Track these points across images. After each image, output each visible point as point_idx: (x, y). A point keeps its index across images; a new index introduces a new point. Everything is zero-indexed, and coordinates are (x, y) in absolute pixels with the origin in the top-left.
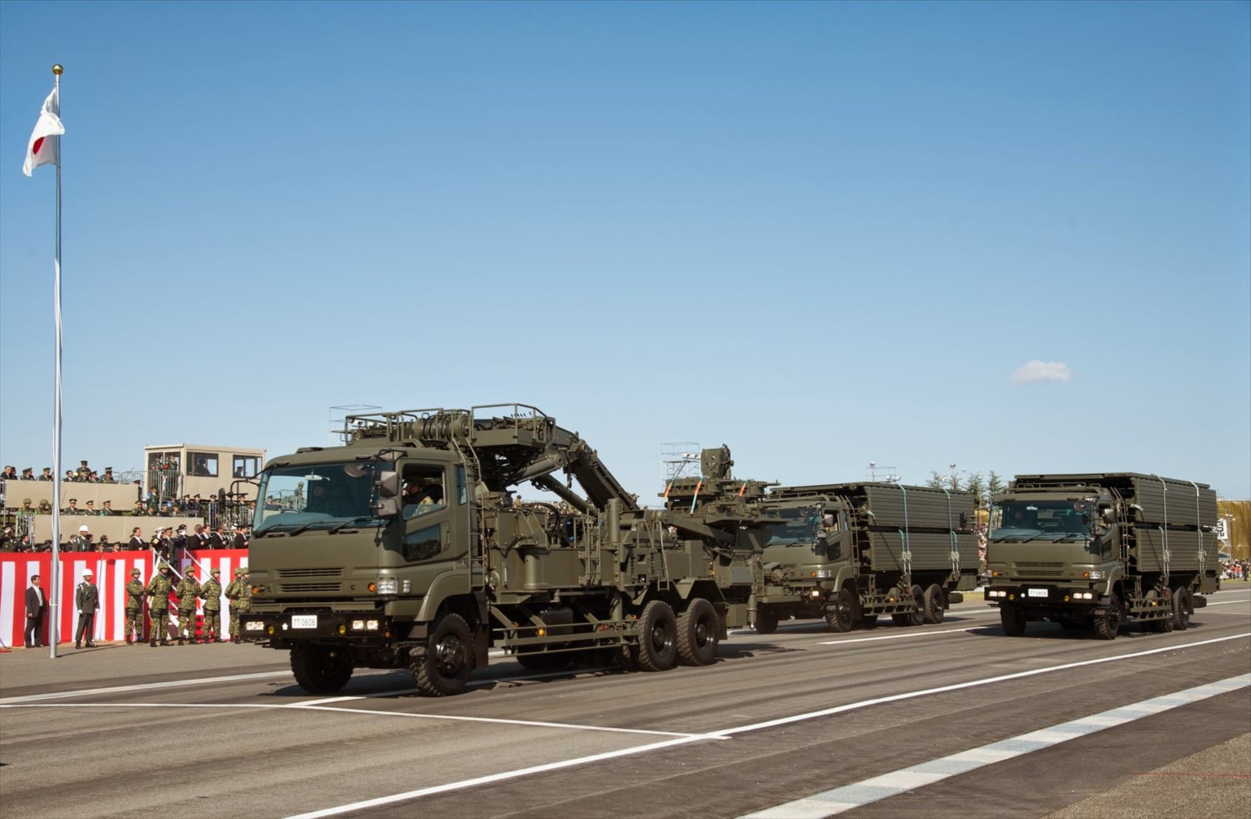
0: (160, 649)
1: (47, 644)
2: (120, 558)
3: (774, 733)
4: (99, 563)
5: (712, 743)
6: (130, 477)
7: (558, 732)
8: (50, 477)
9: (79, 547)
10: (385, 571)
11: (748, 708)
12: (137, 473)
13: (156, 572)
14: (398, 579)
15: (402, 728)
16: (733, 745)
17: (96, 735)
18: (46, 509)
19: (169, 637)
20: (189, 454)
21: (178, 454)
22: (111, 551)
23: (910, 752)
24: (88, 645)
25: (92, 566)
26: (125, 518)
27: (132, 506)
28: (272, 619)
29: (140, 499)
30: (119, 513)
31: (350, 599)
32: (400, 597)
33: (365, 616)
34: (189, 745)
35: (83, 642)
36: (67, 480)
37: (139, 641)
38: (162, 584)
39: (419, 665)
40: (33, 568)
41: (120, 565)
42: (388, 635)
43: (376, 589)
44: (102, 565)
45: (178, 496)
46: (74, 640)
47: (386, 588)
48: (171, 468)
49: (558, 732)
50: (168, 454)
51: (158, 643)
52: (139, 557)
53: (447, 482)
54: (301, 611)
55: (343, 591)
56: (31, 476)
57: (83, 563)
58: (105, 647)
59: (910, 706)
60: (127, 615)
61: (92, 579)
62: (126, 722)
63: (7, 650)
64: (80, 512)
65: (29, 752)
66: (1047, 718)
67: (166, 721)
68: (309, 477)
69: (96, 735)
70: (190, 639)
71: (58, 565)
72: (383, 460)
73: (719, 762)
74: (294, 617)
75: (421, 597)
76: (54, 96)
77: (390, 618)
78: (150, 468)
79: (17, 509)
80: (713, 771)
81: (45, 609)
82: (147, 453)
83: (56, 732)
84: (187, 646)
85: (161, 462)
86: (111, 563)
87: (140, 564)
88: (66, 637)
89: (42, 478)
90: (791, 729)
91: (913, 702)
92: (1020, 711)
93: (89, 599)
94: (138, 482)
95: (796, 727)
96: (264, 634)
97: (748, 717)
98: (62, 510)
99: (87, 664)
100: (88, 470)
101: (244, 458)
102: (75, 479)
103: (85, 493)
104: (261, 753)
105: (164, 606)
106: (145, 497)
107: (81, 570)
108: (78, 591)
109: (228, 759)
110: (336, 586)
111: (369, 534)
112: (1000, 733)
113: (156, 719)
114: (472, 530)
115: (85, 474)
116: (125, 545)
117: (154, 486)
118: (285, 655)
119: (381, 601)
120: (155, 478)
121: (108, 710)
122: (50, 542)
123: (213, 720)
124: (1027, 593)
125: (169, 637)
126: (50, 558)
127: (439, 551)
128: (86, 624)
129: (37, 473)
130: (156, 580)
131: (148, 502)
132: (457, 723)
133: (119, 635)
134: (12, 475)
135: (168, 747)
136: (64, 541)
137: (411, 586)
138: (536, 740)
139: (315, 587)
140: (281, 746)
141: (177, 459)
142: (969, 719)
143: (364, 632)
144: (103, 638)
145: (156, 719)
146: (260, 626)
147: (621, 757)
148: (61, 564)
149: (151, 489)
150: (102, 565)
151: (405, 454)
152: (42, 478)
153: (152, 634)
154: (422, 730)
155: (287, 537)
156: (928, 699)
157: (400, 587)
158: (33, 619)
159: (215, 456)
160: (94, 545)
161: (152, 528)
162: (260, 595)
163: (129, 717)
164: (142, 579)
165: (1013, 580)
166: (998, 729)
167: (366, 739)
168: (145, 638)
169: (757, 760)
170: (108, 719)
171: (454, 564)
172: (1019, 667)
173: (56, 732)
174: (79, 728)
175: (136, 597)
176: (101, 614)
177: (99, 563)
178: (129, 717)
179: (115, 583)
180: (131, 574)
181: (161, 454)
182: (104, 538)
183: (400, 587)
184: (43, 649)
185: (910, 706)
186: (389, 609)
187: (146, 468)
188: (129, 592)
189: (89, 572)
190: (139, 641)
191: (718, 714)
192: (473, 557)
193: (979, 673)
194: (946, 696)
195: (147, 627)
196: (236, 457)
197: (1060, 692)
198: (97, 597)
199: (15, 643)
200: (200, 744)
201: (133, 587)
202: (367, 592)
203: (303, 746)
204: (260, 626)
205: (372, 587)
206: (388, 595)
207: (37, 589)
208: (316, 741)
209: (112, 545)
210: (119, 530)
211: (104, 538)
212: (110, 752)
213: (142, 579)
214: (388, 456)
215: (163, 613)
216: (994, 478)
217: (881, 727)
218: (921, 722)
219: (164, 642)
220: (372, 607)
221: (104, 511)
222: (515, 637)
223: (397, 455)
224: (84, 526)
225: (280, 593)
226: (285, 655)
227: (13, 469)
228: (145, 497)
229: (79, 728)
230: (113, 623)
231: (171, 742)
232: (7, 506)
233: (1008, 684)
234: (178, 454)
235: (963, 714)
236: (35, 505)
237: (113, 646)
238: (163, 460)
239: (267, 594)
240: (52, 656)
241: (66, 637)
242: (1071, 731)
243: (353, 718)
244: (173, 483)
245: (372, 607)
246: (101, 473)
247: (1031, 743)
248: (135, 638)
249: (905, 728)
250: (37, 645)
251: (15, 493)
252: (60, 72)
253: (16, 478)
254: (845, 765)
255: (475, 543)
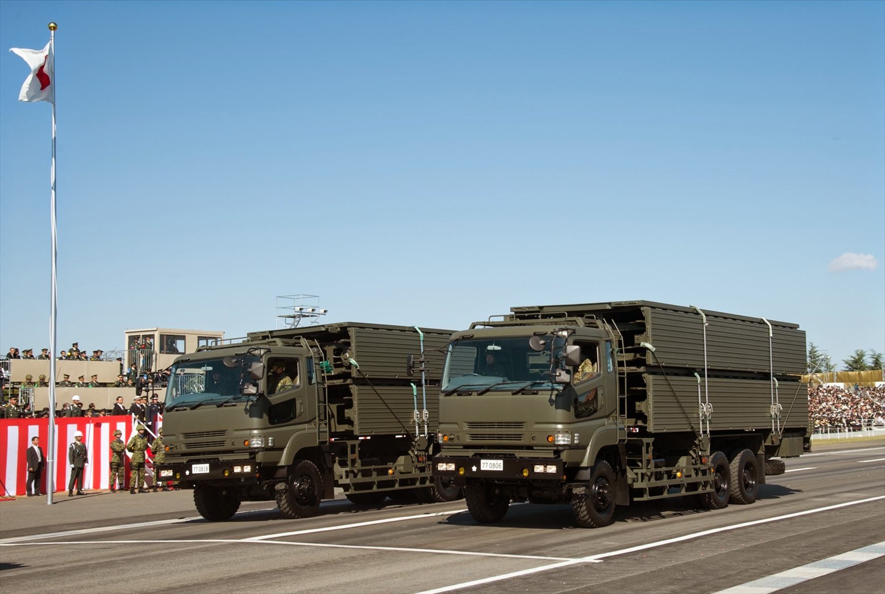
0: (138, 496)
1: (44, 492)
2: (105, 421)
3: (637, 557)
4: (88, 425)
5: (588, 566)
6: (113, 355)
7: (463, 558)
8: (47, 356)
9: (72, 413)
10: (255, 432)
11: (615, 537)
12: (119, 352)
13: (135, 433)
14: (265, 437)
15: (336, 557)
16: (604, 567)
17: (85, 567)
18: (44, 383)
19: (145, 486)
20: (162, 336)
21: (152, 336)
22: (98, 416)
23: (746, 571)
24: (79, 493)
25: (82, 428)
26: (109, 389)
27: (115, 379)
28: (179, 469)
29: (121, 373)
30: (104, 385)
31: (232, 452)
32: (266, 449)
33: (242, 463)
34: (162, 574)
35: (75, 491)
36: (61, 359)
37: (121, 489)
38: (140, 443)
39: (281, 496)
40: (34, 431)
41: (105, 427)
42: (258, 475)
43: (249, 444)
44: (90, 428)
45: (153, 370)
46: (67, 489)
47: (256, 443)
48: (147, 348)
49: (463, 558)
50: (145, 337)
51: (136, 491)
52: (121, 421)
53: (301, 367)
54: (198, 462)
55: (228, 446)
56: (32, 356)
57: (75, 426)
58: (94, 494)
59: (747, 533)
60: (111, 468)
61: (82, 439)
62: (111, 556)
63: (12, 499)
64: (72, 384)
65: (29, 583)
66: (856, 541)
67: (143, 555)
68: (204, 368)
69: (85, 567)
70: (163, 487)
71: (53, 429)
72: (254, 355)
73: (592, 581)
74: (194, 466)
75: (282, 449)
76: (50, 49)
77: (259, 464)
78: (130, 347)
79: (20, 383)
80: (589, 588)
81: (44, 463)
82: (127, 335)
83: (52, 565)
84: (160, 493)
85: (139, 343)
86: (98, 426)
87: (121, 426)
88: (61, 487)
89: (41, 357)
90: (651, 553)
91: (749, 530)
92: (834, 536)
93: (79, 455)
94: (120, 359)
95: (655, 552)
96: (173, 478)
97: (617, 544)
98: (57, 383)
99: (78, 509)
100: (77, 350)
101: (206, 338)
102: (68, 358)
103: (76, 369)
104: (221, 579)
105: (141, 460)
106: (126, 371)
107: (73, 432)
108: (71, 449)
109: (195, 585)
110: (222, 443)
111: (242, 406)
112: (819, 554)
113: (134, 553)
114: (319, 402)
115: (76, 354)
116: (110, 411)
117: (133, 363)
118: (189, 494)
119: (253, 452)
120: (134, 356)
121: (96, 546)
122: (48, 409)
123: (182, 554)
124: (478, 466)
125: (145, 486)
126: (48, 423)
127: (295, 417)
128: (77, 476)
129: (37, 353)
130: (135, 439)
131: (128, 375)
132: (381, 553)
133: (105, 484)
134: (15, 355)
135: (143, 576)
136: (59, 408)
137: (273, 441)
138: (445, 565)
139: (208, 444)
140: (238, 573)
141: (152, 340)
142: (794, 543)
143: (242, 474)
144: (91, 487)
145: (134, 553)
146: (170, 473)
147: (514, 578)
148: (56, 427)
149: (130, 365)
150: (90, 428)
151: (269, 351)
152: (41, 357)
153: (132, 483)
154: (352, 559)
155: (189, 411)
156: (761, 527)
157: (267, 442)
158: (35, 473)
159: (183, 338)
160: (84, 411)
161: (129, 397)
162: (170, 452)
163: (112, 552)
164: (123, 438)
165: (466, 447)
166: (817, 551)
167: (307, 567)
168: (126, 487)
169: (624, 579)
170: (95, 554)
171: (306, 426)
172: (834, 500)
173: (52, 565)
174: (71, 562)
175: (117, 453)
176: (89, 468)
177: (88, 425)
178: (112, 552)
179: (100, 443)
180: (114, 435)
181: (138, 337)
182: (91, 406)
183: (573, 439)
184: (41, 497)
185: (747, 533)
186: (259, 458)
187: (127, 348)
188: (112, 450)
189: (80, 434)
190: (121, 489)
191: (593, 542)
192: (320, 420)
193: (803, 506)
194: (774, 525)
195: (128, 478)
196: (200, 338)
197: (867, 520)
198: (86, 453)
199: (18, 493)
200: (171, 573)
201: (116, 445)
202: (242, 446)
203: (256, 574)
204: (170, 473)
205: (246, 443)
206: (564, 445)
207: (36, 448)
208: (266, 569)
209: (99, 411)
210: (105, 399)
211: (91, 406)
212: (96, 581)
213: (123, 438)
214: (257, 352)
215: (141, 466)
216: (813, 348)
217: (724, 551)
218: (756, 546)
219: (141, 490)
220: (247, 456)
221: (92, 383)
222: (359, 476)
223: (262, 352)
224: (75, 396)
225: (184, 449)
226: (189, 494)
227: (17, 350)
228: (126, 371)
229: (71, 562)
230: (100, 475)
231: (147, 572)
232: (11, 380)
233: (826, 514)
234: (152, 336)
235: (790, 539)
236: (35, 379)
237: (100, 494)
238: (140, 341)
239: (175, 451)
240: (49, 503)
241: (61, 487)
242: (876, 552)
243: (296, 550)
244: (148, 360)
245: (552, 456)
246: (90, 354)
247: (842, 561)
248: (117, 487)
249: (743, 551)
250: (37, 494)
251: (17, 372)
252: (55, 28)
253: (19, 357)
254: (695, 582)
255: (322, 410)
